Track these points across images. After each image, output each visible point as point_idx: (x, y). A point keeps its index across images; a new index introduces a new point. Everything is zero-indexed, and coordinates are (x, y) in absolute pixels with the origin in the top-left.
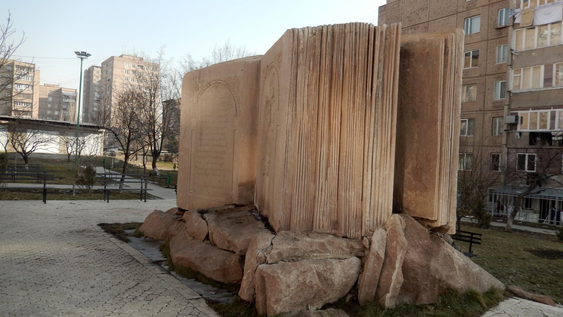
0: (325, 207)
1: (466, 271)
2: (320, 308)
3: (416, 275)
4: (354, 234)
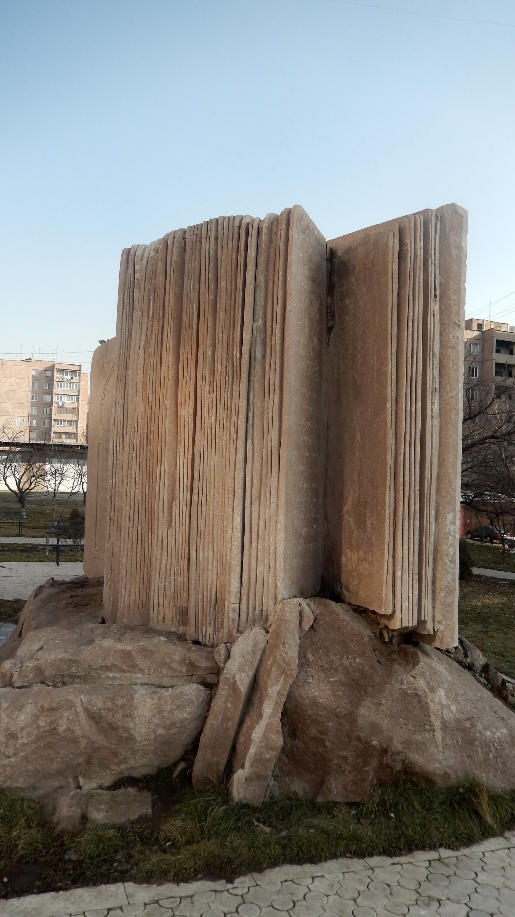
0: (168, 579)
1: (465, 735)
2: (106, 785)
3: (321, 733)
4: (211, 635)
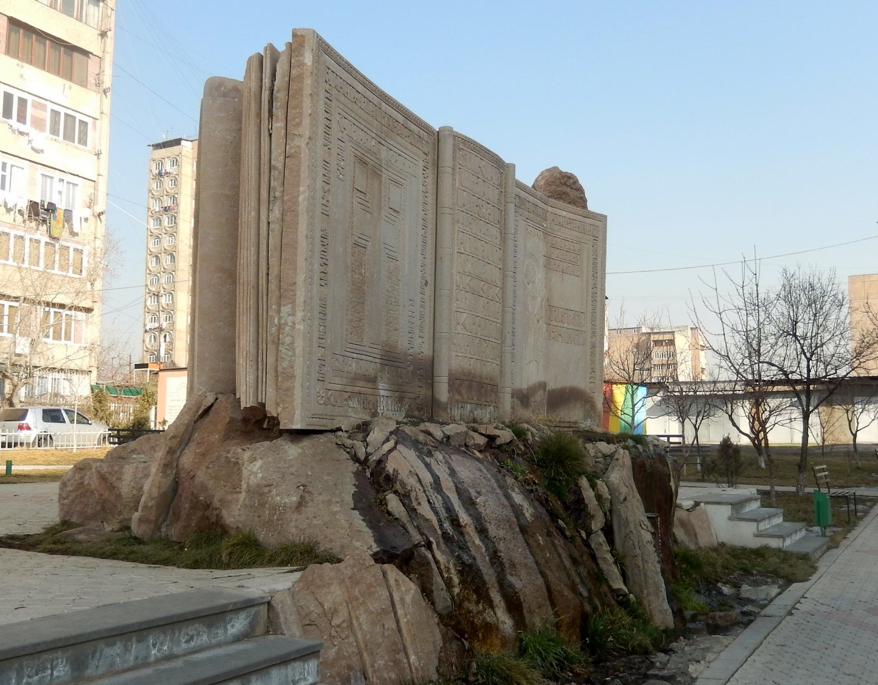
2: (115, 529)
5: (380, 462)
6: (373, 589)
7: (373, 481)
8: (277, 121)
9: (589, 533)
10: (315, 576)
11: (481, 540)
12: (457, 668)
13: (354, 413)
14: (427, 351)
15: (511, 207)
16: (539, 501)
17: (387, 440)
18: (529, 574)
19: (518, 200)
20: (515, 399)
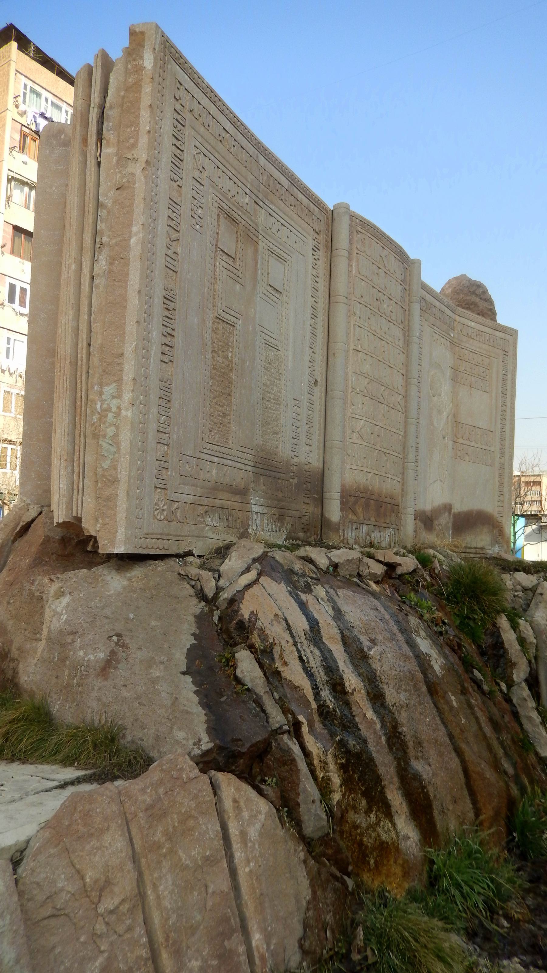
5: (232, 601)
6: (191, 823)
7: (221, 629)
8: (108, 145)
9: (510, 684)
10: (76, 816)
11: (375, 711)
12: (333, 932)
13: (214, 532)
14: (315, 462)
15: (416, 308)
16: (450, 646)
17: (248, 570)
18: (441, 754)
19: (423, 304)
20: (418, 521)
